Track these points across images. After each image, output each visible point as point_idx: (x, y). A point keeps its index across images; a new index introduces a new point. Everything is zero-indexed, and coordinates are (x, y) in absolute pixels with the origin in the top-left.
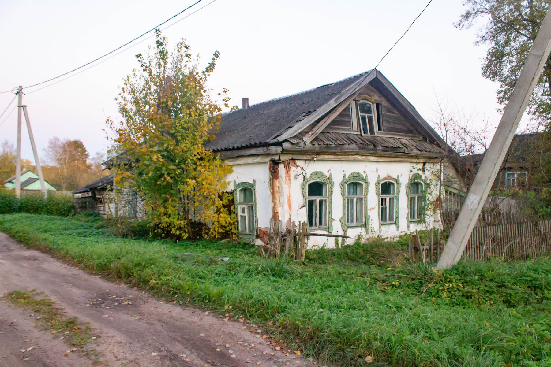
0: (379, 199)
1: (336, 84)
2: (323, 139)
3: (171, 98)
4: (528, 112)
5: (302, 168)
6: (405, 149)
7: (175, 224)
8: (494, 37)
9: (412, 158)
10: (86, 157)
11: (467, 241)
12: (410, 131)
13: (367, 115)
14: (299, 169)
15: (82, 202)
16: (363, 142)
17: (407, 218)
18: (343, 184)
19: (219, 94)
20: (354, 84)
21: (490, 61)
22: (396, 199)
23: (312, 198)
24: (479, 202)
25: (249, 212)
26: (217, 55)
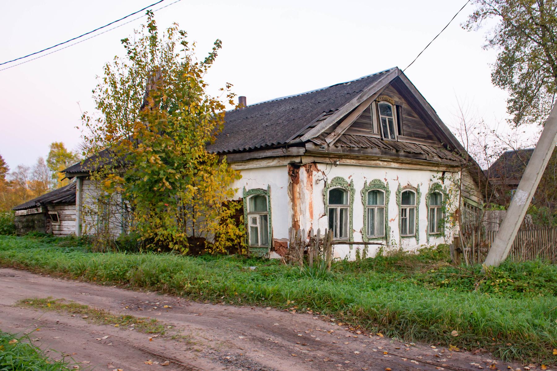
0: (399, 209)
1: (352, 82)
2: (346, 142)
3: (165, 91)
4: (539, 124)
5: (323, 173)
6: (427, 155)
7: (174, 237)
8: (504, 41)
9: (433, 166)
10: (5, 172)
11: (514, 237)
12: (429, 138)
13: (387, 118)
14: (320, 173)
15: (27, 221)
16: (385, 147)
17: (427, 231)
18: (364, 192)
19: (222, 89)
20: (376, 83)
21: (501, 67)
22: (416, 209)
23: (333, 206)
24: (528, 198)
25: (261, 224)
26: (218, 44)
